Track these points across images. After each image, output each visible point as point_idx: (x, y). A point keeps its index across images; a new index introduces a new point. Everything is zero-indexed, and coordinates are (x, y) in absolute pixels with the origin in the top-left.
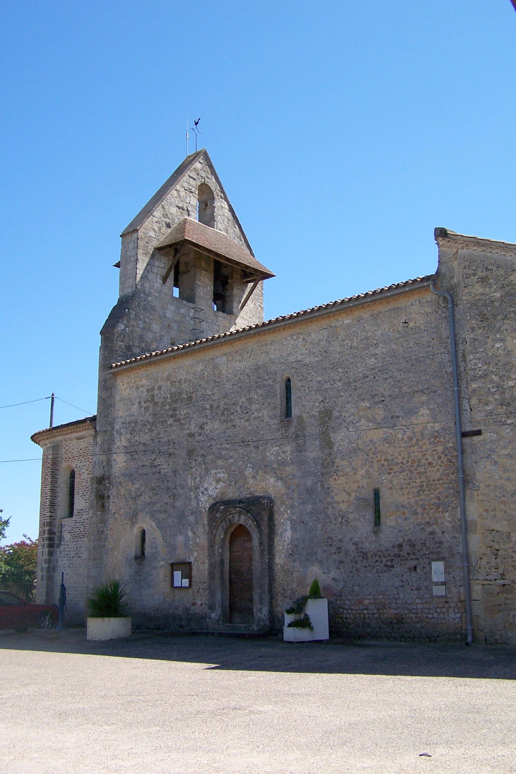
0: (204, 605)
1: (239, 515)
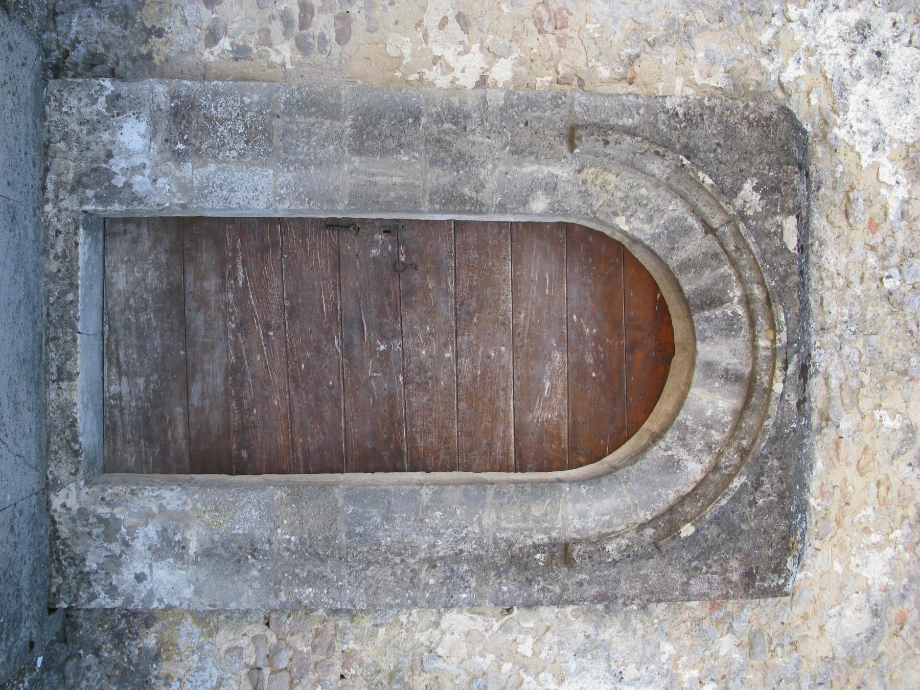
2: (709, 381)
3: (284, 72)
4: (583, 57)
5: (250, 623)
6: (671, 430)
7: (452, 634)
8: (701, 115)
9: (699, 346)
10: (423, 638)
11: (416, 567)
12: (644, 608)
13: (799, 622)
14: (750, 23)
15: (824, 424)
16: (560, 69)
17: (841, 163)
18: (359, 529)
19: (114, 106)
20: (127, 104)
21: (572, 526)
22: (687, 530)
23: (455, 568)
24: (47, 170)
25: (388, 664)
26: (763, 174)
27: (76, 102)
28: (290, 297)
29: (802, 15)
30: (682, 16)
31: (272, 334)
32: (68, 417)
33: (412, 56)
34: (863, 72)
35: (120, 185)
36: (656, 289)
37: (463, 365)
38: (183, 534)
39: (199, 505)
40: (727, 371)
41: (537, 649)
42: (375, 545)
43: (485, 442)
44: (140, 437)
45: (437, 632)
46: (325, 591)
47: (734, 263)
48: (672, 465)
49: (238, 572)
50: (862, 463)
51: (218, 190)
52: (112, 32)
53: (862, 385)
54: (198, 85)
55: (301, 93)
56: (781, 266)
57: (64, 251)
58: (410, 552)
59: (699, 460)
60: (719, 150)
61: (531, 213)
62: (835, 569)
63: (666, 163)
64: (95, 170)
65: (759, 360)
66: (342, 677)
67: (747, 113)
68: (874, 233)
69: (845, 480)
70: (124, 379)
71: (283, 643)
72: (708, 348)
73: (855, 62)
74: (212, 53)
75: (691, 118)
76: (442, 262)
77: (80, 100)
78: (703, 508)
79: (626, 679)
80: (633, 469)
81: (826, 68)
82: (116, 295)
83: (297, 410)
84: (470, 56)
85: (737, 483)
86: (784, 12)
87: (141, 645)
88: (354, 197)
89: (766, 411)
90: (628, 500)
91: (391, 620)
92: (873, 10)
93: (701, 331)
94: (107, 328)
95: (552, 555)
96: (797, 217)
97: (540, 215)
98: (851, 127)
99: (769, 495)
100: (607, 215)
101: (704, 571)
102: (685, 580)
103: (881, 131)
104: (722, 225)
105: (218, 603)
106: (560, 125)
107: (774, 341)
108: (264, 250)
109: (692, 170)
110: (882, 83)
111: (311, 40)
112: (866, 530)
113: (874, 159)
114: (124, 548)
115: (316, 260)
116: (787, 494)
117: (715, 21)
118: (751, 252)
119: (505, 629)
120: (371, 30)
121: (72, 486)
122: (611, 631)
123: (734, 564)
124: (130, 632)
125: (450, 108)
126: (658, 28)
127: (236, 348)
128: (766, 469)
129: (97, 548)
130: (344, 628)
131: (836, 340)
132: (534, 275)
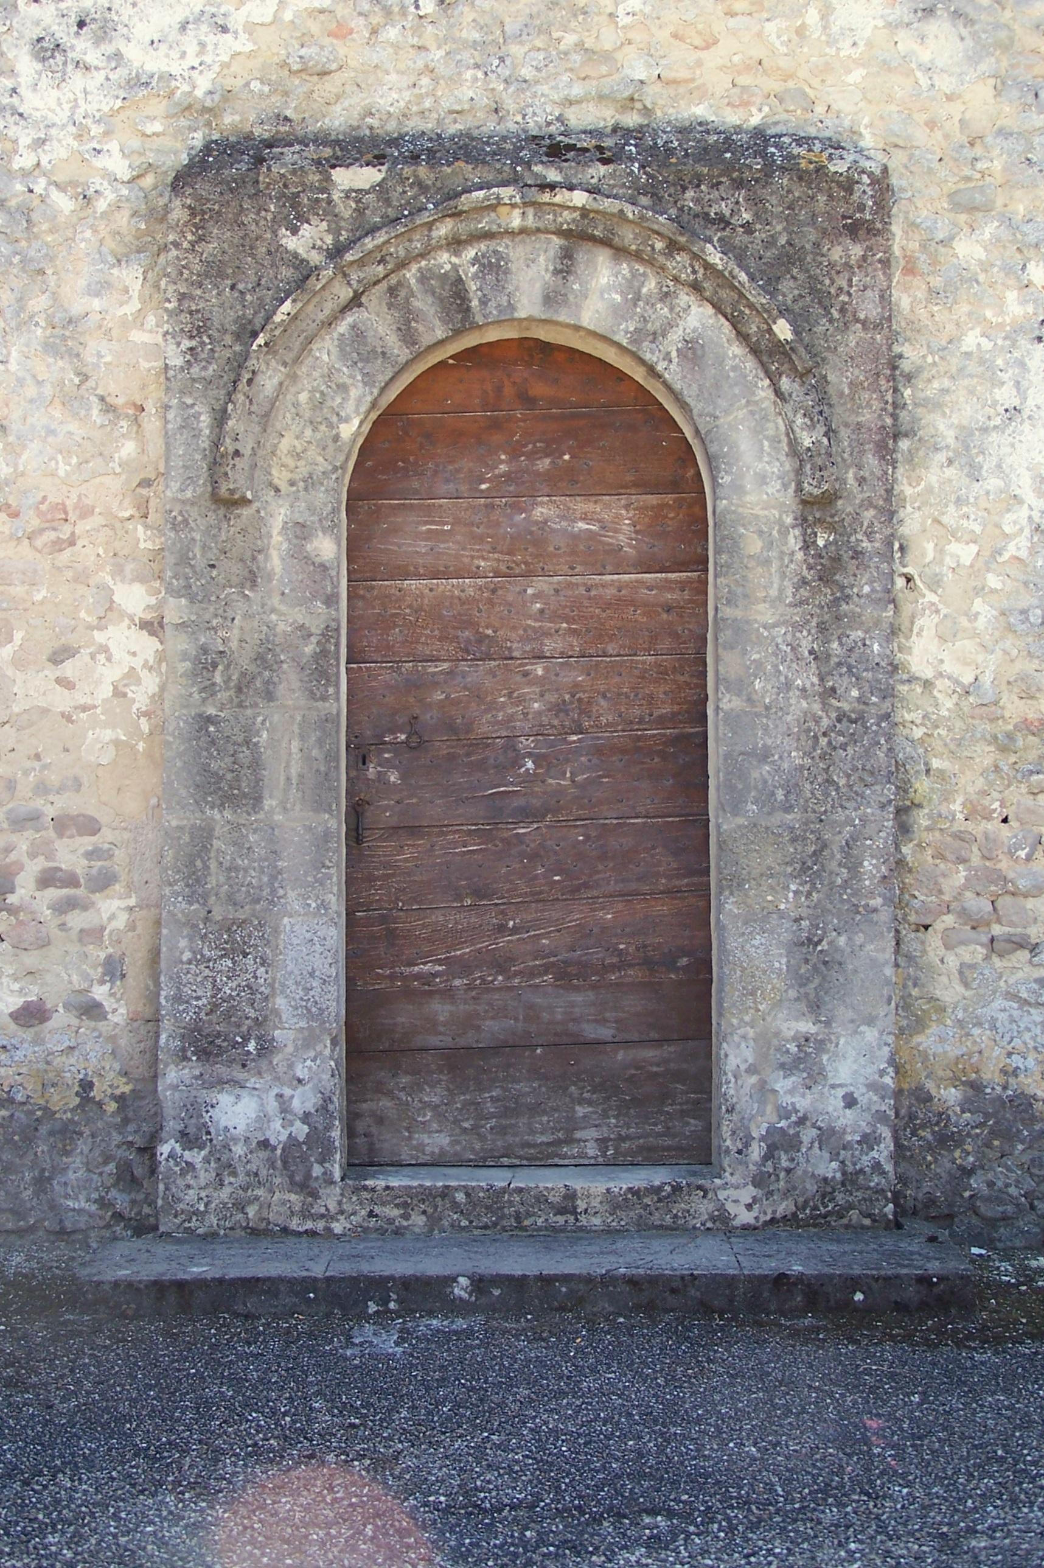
0: (61, 1018)
1: (567, 255)
2: (571, 298)
3: (141, 908)
4: (107, 480)
5: (924, 952)
6: (640, 353)
7: (942, 661)
8: (191, 313)
9: (521, 314)
10: (947, 704)
11: (834, 715)
12: (909, 378)
13: (938, 134)
14: (45, 227)
15: (638, 105)
16: (127, 514)
17: (247, 84)
18: (780, 795)
19: (197, 1139)
20: (193, 1121)
21: (777, 495)
22: (783, 330)
23: (837, 660)
24: (285, 1230)
25: (985, 755)
26: (274, 220)
27: (191, 1192)
28: (459, 897)
29: (29, 147)
30: (39, 331)
31: (511, 923)
32: (626, 1200)
33: (114, 728)
34: (109, 49)
35: (306, 1129)
36: (442, 364)
37: (555, 649)
38: (787, 1041)
39: (747, 1018)
40: (556, 272)
41: (966, 537)
42: (802, 772)
43: (665, 616)
44: (661, 1112)
45: (938, 683)
46: (868, 842)
47: (403, 264)
48: (692, 351)
49: (840, 964)
50: (698, 42)
51: (312, 993)
52: (86, 1150)
53: (580, 46)
54: (167, 1024)
55: (176, 882)
56: (405, 192)
57: (397, 1206)
58: (812, 724)
59: (685, 310)
60: (241, 286)
61: (338, 558)
62: (859, 80)
63: (263, 367)
64: (285, 1163)
65: (541, 225)
66: (1005, 820)
67: (185, 245)
68: (351, 32)
69: (721, 68)
70: (578, 1135)
71: (953, 906)
72: (525, 301)
73: (96, 63)
74: (115, 1010)
75: (199, 328)
76: (407, 680)
77: (188, 1187)
78: (751, 306)
79: (1016, 402)
80: (697, 406)
81: (106, 109)
82: (458, 1148)
83: (620, 887)
84: (111, 645)
85: (715, 258)
86: (25, 174)
87: (958, 1109)
88: (320, 806)
89: (613, 215)
90: (741, 414)
91: (921, 751)
92: (15, 34)
93: (500, 312)
94: (505, 1161)
95: (820, 521)
96: (333, 167)
97: (339, 545)
98: (193, 68)
99: (737, 203)
100: (339, 450)
101: (846, 299)
102: (859, 326)
103: (197, 21)
104: (349, 283)
105: (885, 992)
106: (212, 518)
107: (513, 206)
108: (392, 935)
109: (272, 330)
110: (125, 19)
111: (94, 871)
112: (801, 32)
113: (240, 31)
114: (808, 1123)
115: (406, 860)
116: (735, 175)
117: (44, 282)
118: (388, 242)
119: (935, 584)
120: (78, 785)
121: (722, 1195)
122: (943, 427)
123: (836, 254)
124: (937, 1124)
125: (194, 674)
126: (57, 370)
127: (532, 973)
128: (698, 209)
129: (808, 1161)
130: (930, 816)
131: (512, 89)
132: (423, 546)
